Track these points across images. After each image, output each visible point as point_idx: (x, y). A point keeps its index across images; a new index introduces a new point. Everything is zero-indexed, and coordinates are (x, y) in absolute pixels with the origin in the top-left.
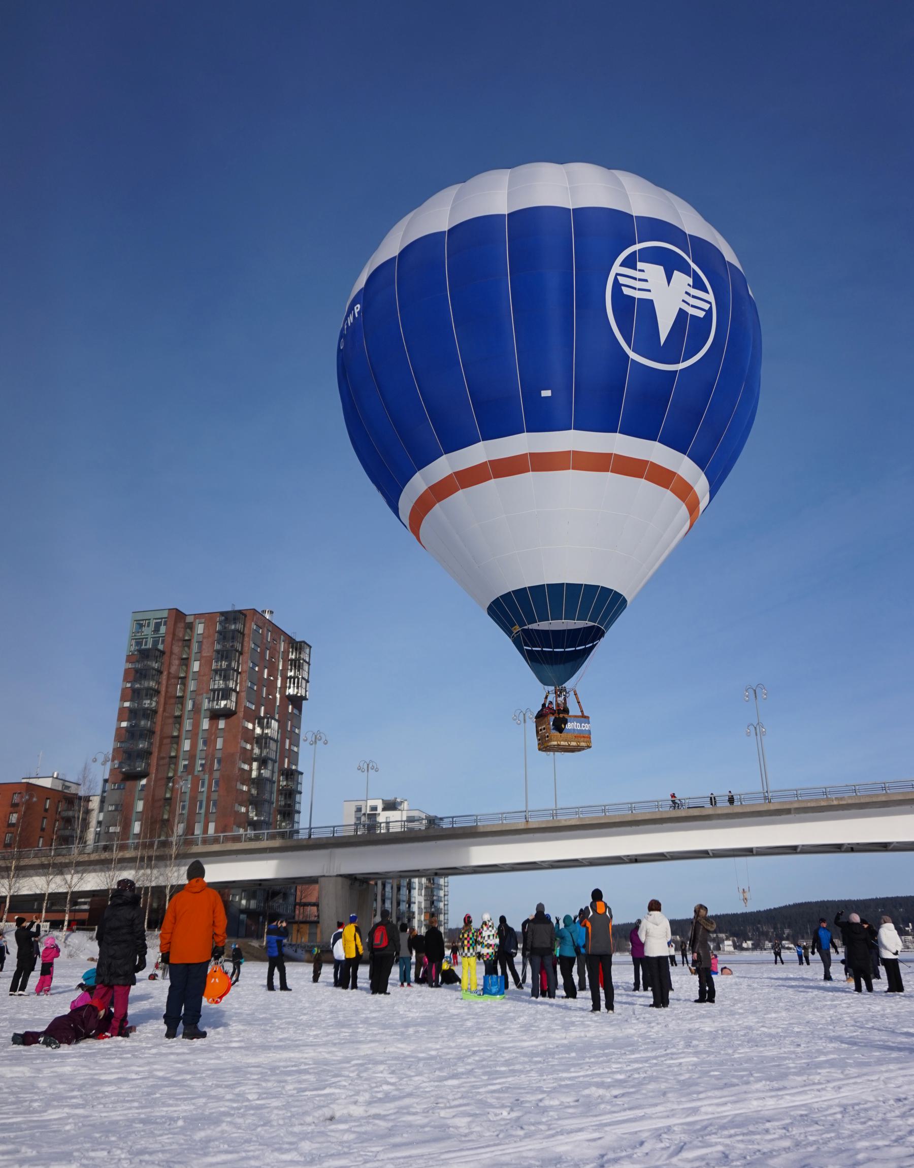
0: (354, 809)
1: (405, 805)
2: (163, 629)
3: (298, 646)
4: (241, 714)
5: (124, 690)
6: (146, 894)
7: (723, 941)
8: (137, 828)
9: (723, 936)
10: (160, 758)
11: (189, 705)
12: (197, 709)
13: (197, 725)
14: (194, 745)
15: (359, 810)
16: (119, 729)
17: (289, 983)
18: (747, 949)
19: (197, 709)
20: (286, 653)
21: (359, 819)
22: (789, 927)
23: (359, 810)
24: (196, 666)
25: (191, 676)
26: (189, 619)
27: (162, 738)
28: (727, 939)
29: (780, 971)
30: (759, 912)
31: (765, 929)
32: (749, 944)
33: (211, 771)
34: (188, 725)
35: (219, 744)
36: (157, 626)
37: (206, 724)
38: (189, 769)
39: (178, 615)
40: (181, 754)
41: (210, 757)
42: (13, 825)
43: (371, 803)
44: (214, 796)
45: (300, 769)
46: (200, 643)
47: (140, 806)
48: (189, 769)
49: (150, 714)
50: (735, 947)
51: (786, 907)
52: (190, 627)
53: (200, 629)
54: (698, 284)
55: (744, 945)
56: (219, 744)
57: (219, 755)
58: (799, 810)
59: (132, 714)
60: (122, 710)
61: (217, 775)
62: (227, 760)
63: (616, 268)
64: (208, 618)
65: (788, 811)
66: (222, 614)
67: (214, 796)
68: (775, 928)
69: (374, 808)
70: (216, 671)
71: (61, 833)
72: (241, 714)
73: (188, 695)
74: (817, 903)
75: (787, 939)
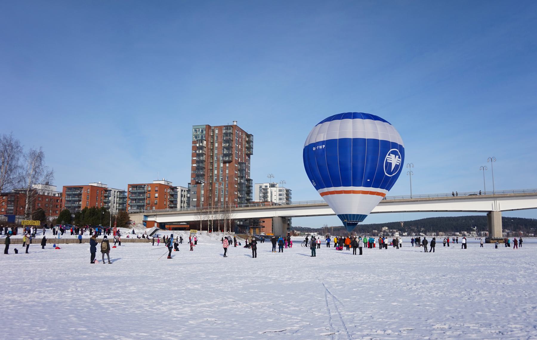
1: (278, 185)
2: (204, 132)
3: (249, 136)
4: (234, 162)
5: (193, 153)
6: (228, 223)
7: (395, 232)
8: (203, 199)
9: (395, 230)
10: (208, 177)
11: (215, 159)
12: (218, 160)
13: (219, 165)
14: (218, 172)
15: (261, 187)
16: (192, 167)
17: (29, 250)
18: (405, 236)
19: (218, 160)
20: (245, 138)
21: (261, 190)
22: (424, 227)
23: (261, 187)
24: (216, 145)
25: (215, 148)
26: (213, 128)
27: (208, 170)
28: (397, 232)
29: (153, 247)
30: (411, 221)
31: (413, 228)
32: (406, 234)
33: (225, 181)
34: (215, 165)
35: (227, 172)
36: (202, 131)
37: (222, 165)
38: (217, 180)
39: (209, 127)
40: (214, 175)
41: (224, 176)
42: (157, 197)
44: (227, 189)
45: (251, 178)
46: (217, 137)
47: (203, 192)
48: (217, 180)
49: (202, 162)
50: (400, 235)
51: (423, 219)
52: (213, 131)
53: (217, 131)
54: (399, 158)
55: (404, 234)
56: (227, 172)
57: (227, 175)
58: (420, 201)
59: (198, 162)
60: (193, 160)
61: (227, 182)
62: (230, 177)
63: (387, 156)
64: (220, 128)
65: (417, 201)
66: (225, 126)
67: (227, 189)
68: (417, 228)
69: (266, 186)
70: (224, 147)
71: (170, 199)
72: (234, 162)
73: (215, 155)
74: (436, 218)
75: (422, 232)
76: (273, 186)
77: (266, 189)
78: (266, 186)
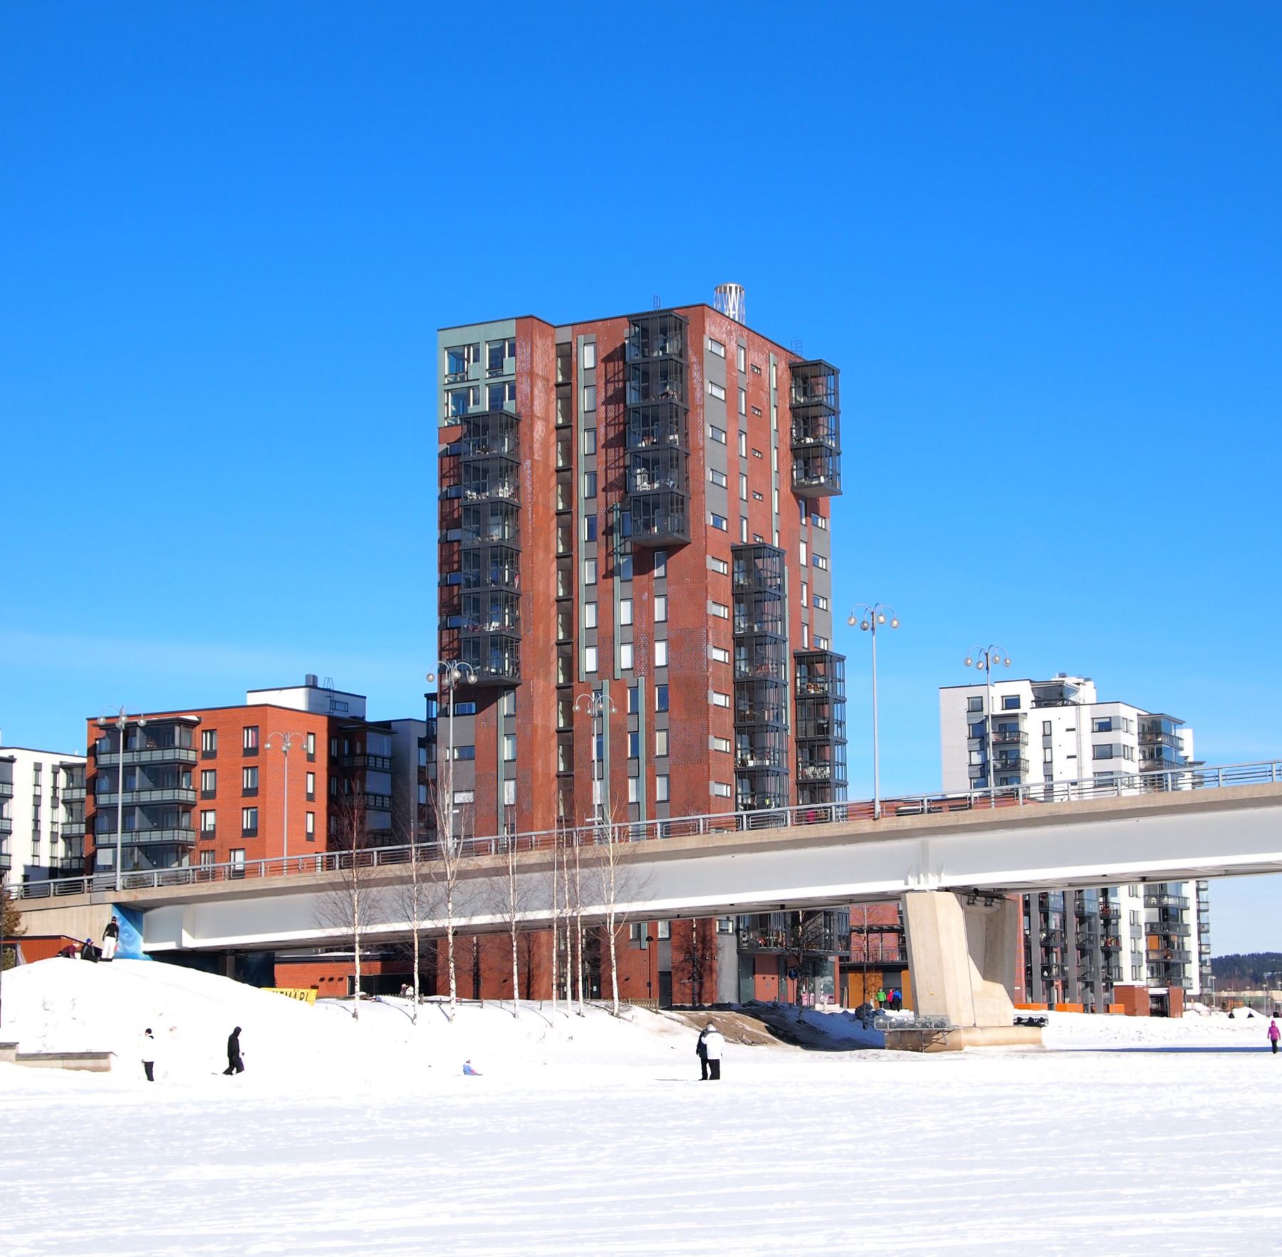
0: (965, 705)
43: (1010, 689)
69: (1012, 702)
76: (1051, 696)
77: (1008, 728)
78: (1012, 702)
